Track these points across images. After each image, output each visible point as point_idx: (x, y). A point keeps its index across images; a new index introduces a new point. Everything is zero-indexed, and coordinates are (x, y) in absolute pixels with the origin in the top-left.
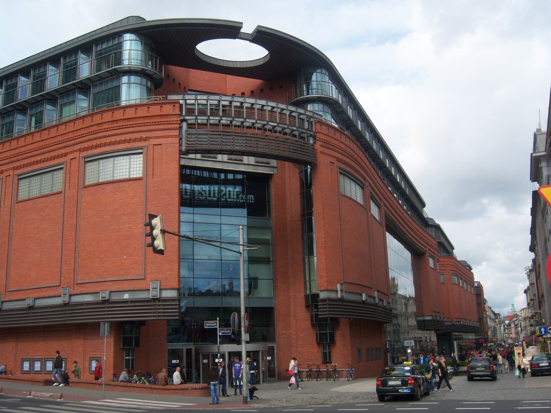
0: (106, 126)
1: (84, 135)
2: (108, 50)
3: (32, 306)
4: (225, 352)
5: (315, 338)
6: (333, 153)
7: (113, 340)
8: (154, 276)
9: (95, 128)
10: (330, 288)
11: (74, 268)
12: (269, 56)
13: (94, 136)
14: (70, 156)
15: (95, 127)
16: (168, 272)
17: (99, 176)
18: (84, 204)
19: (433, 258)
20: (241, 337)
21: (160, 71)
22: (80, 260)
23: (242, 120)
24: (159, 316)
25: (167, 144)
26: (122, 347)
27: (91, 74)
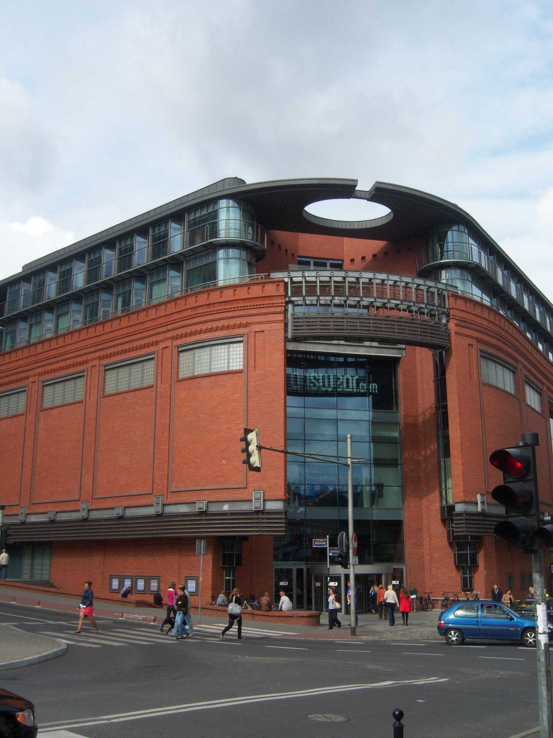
0: (201, 310)
1: (177, 321)
2: (204, 220)
3: (122, 516)
4: (341, 574)
5: (453, 560)
6: (472, 333)
7: (211, 557)
8: (256, 485)
9: (189, 313)
10: (467, 499)
11: (168, 474)
12: (392, 215)
13: (188, 322)
14: (162, 345)
15: (189, 311)
16: (273, 480)
17: (194, 369)
18: (179, 400)
19: (540, 393)
20: (348, 560)
21: (262, 242)
22: (174, 465)
23: (358, 299)
24: (263, 531)
25: (270, 330)
26: (221, 566)
27: (184, 249)
